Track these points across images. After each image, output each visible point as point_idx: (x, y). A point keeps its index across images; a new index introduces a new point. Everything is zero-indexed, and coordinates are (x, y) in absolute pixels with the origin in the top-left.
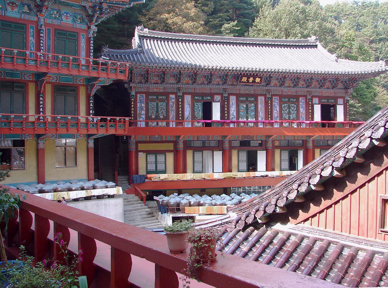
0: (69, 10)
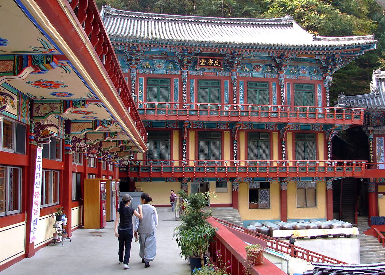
0: (306, 66)
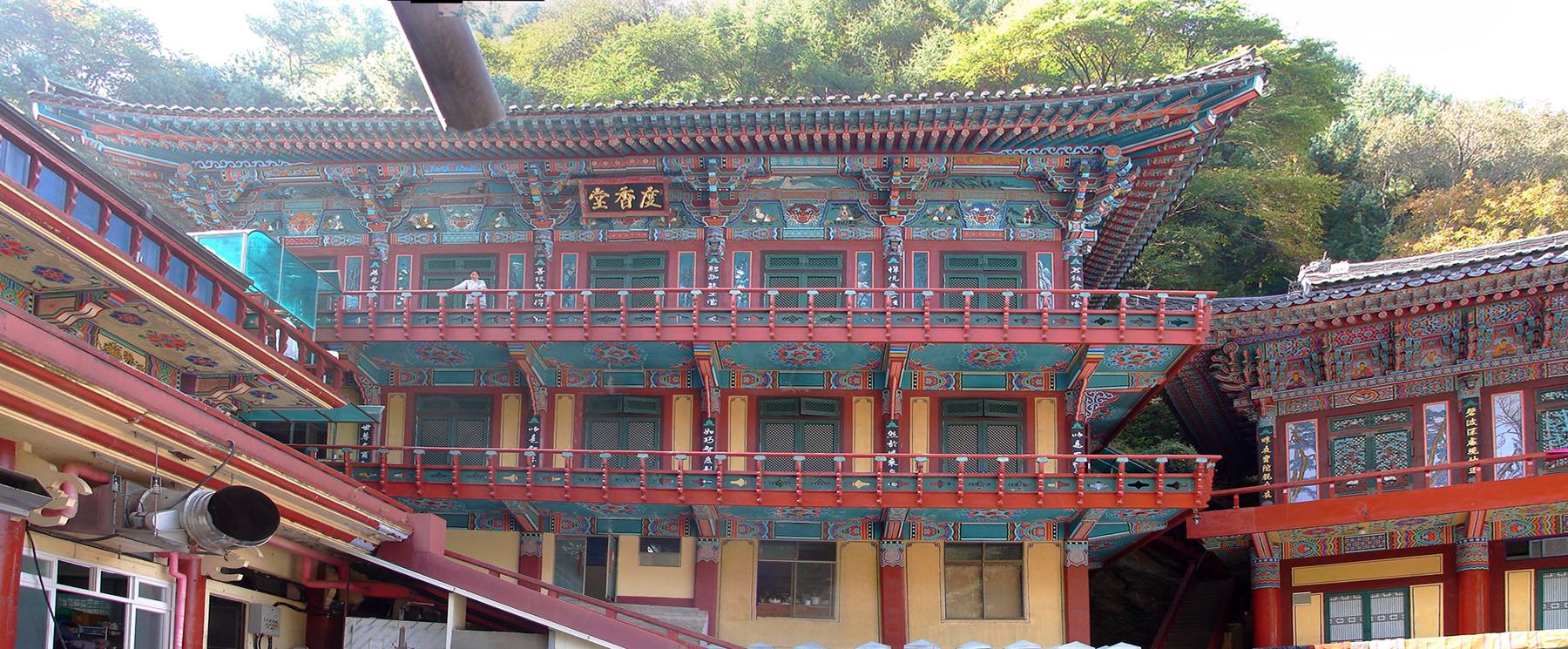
0: (990, 197)
